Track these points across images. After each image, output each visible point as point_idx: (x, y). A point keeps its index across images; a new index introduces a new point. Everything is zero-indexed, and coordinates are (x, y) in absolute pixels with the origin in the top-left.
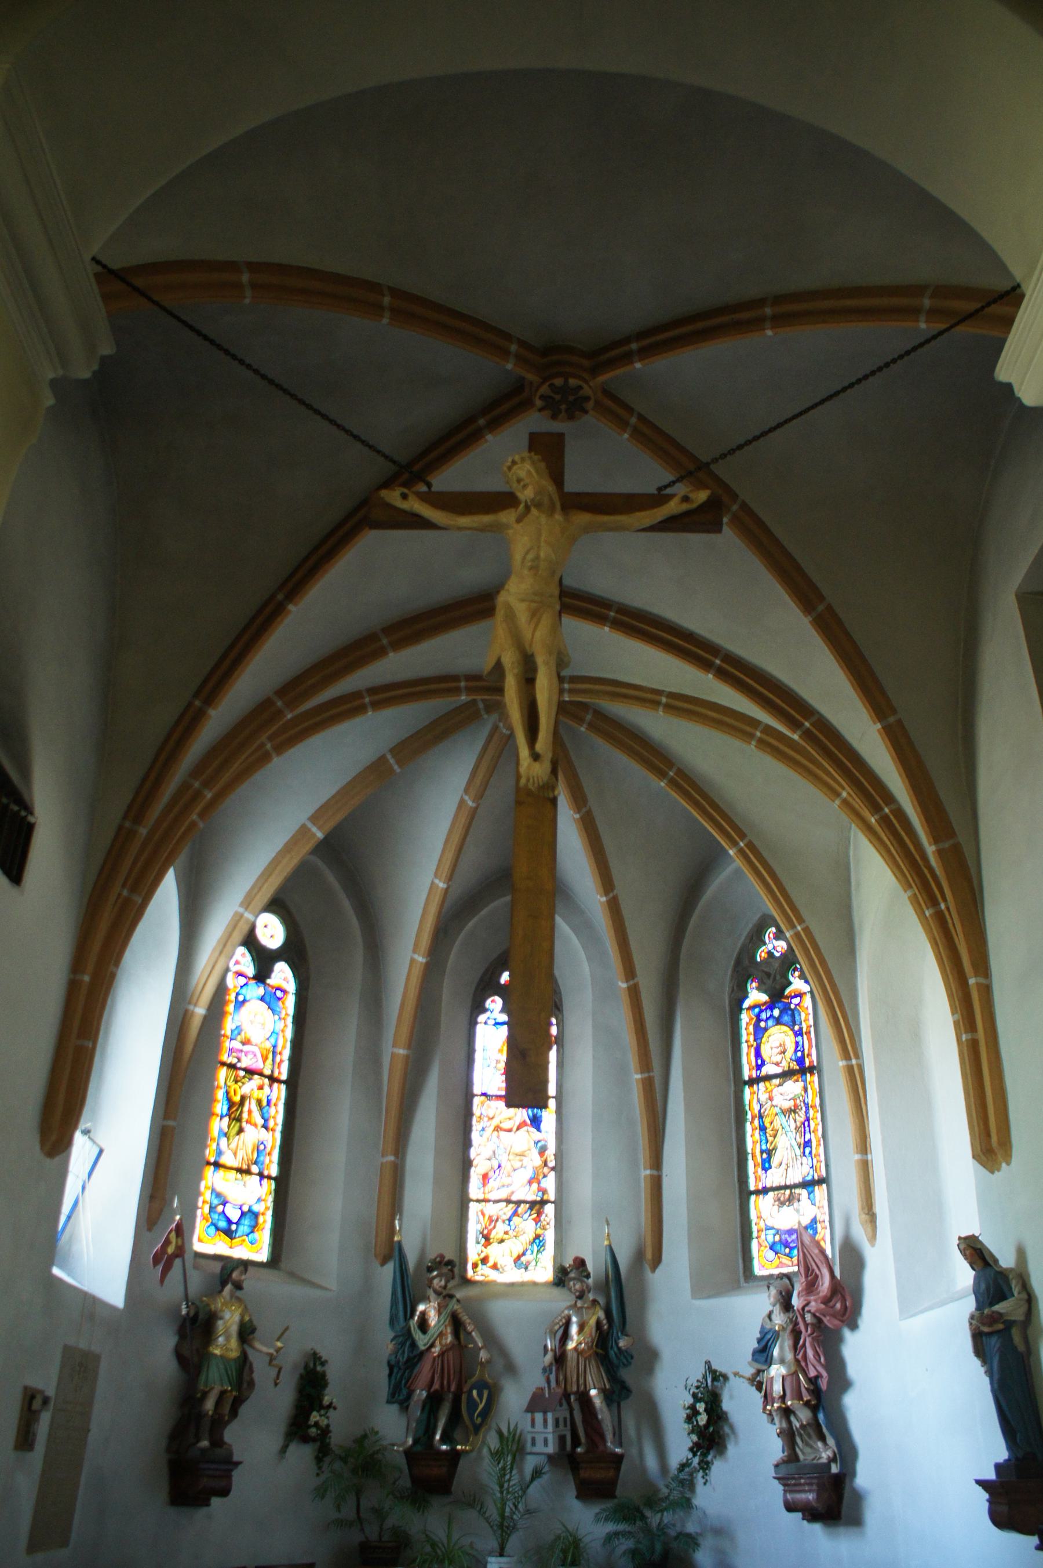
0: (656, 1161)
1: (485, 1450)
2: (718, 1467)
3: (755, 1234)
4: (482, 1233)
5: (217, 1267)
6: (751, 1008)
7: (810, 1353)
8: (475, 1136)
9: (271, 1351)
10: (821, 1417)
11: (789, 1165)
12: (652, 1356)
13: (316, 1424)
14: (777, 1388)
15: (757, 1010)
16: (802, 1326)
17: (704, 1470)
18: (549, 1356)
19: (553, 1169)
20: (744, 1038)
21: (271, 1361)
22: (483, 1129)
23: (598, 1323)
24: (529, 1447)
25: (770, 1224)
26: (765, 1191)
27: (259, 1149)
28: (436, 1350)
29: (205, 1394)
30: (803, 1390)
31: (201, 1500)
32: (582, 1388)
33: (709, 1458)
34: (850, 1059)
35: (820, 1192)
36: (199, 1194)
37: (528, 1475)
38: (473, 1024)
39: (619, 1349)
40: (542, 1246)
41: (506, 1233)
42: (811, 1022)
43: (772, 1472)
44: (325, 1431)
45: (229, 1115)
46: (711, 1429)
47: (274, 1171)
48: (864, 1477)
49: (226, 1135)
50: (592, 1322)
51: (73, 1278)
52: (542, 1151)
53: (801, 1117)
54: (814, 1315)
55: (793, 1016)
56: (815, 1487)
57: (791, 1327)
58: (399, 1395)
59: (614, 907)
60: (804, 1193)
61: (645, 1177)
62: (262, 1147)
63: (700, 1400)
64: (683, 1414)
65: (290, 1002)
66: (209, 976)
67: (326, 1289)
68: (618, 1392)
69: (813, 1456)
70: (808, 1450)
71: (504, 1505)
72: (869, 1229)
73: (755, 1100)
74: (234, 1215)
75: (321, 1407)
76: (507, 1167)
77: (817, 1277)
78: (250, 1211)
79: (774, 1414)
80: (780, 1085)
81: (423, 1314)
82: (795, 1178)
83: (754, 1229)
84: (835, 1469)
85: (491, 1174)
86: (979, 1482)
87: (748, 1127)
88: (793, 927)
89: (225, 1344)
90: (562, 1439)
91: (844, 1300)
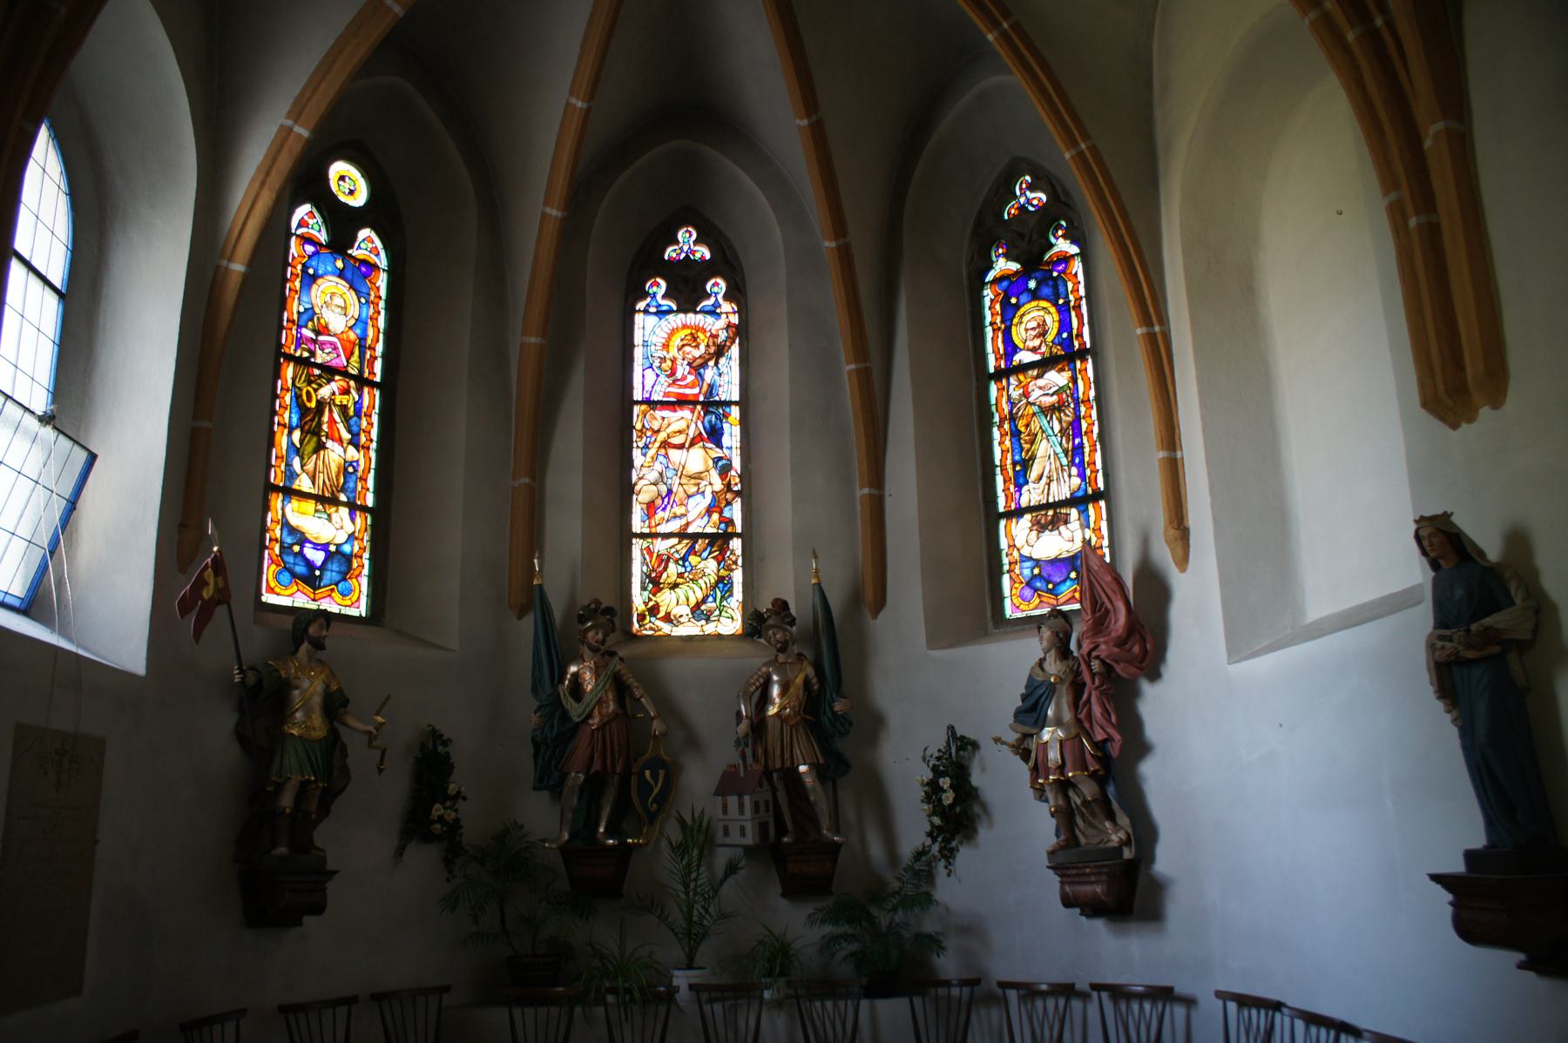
0: (876, 475)
1: (664, 843)
2: (965, 856)
3: (1006, 568)
4: (648, 576)
5: (288, 622)
6: (996, 281)
7: (1097, 710)
8: (638, 457)
9: (370, 728)
10: (1111, 790)
11: (1050, 478)
12: (875, 723)
13: (441, 819)
14: (1054, 755)
15: (1005, 284)
16: (1087, 677)
17: (946, 858)
18: (744, 726)
19: (738, 494)
20: (988, 319)
21: (370, 742)
22: (646, 446)
23: (807, 682)
24: (720, 838)
25: (1026, 552)
26: (1019, 512)
27: (347, 469)
28: (595, 721)
29: (280, 787)
30: (1088, 757)
31: (292, 918)
32: (788, 764)
33: (954, 844)
34: (1152, 325)
35: (1097, 512)
36: (264, 529)
37: (720, 872)
38: (631, 312)
39: (834, 714)
40: (728, 592)
41: (680, 575)
42: (1082, 292)
43: (1045, 860)
44: (454, 828)
45: (301, 426)
46: (958, 810)
47: (370, 501)
48: (1165, 862)
49: (298, 452)
50: (799, 680)
51: (70, 639)
52: (724, 471)
53: (1068, 417)
54: (1103, 662)
55: (1056, 287)
56: (1104, 878)
57: (1070, 678)
58: (549, 778)
59: (818, 136)
60: (1074, 513)
61: (863, 496)
62: (351, 470)
63: (943, 774)
64: (921, 793)
65: (382, 281)
66: (247, 218)
67: (439, 647)
68: (832, 768)
69: (1098, 839)
70: (1091, 831)
71: (691, 908)
72: (1179, 550)
73: (1004, 400)
74: (317, 557)
75: (445, 797)
76: (679, 494)
77: (1107, 611)
78: (338, 552)
79: (1047, 788)
80: (1040, 376)
81: (576, 675)
82: (1061, 491)
83: (1005, 561)
84: (1128, 854)
85: (659, 502)
86: (1436, 878)
87: (996, 433)
88: (1075, 144)
89: (306, 720)
90: (763, 827)
91: (1143, 639)
